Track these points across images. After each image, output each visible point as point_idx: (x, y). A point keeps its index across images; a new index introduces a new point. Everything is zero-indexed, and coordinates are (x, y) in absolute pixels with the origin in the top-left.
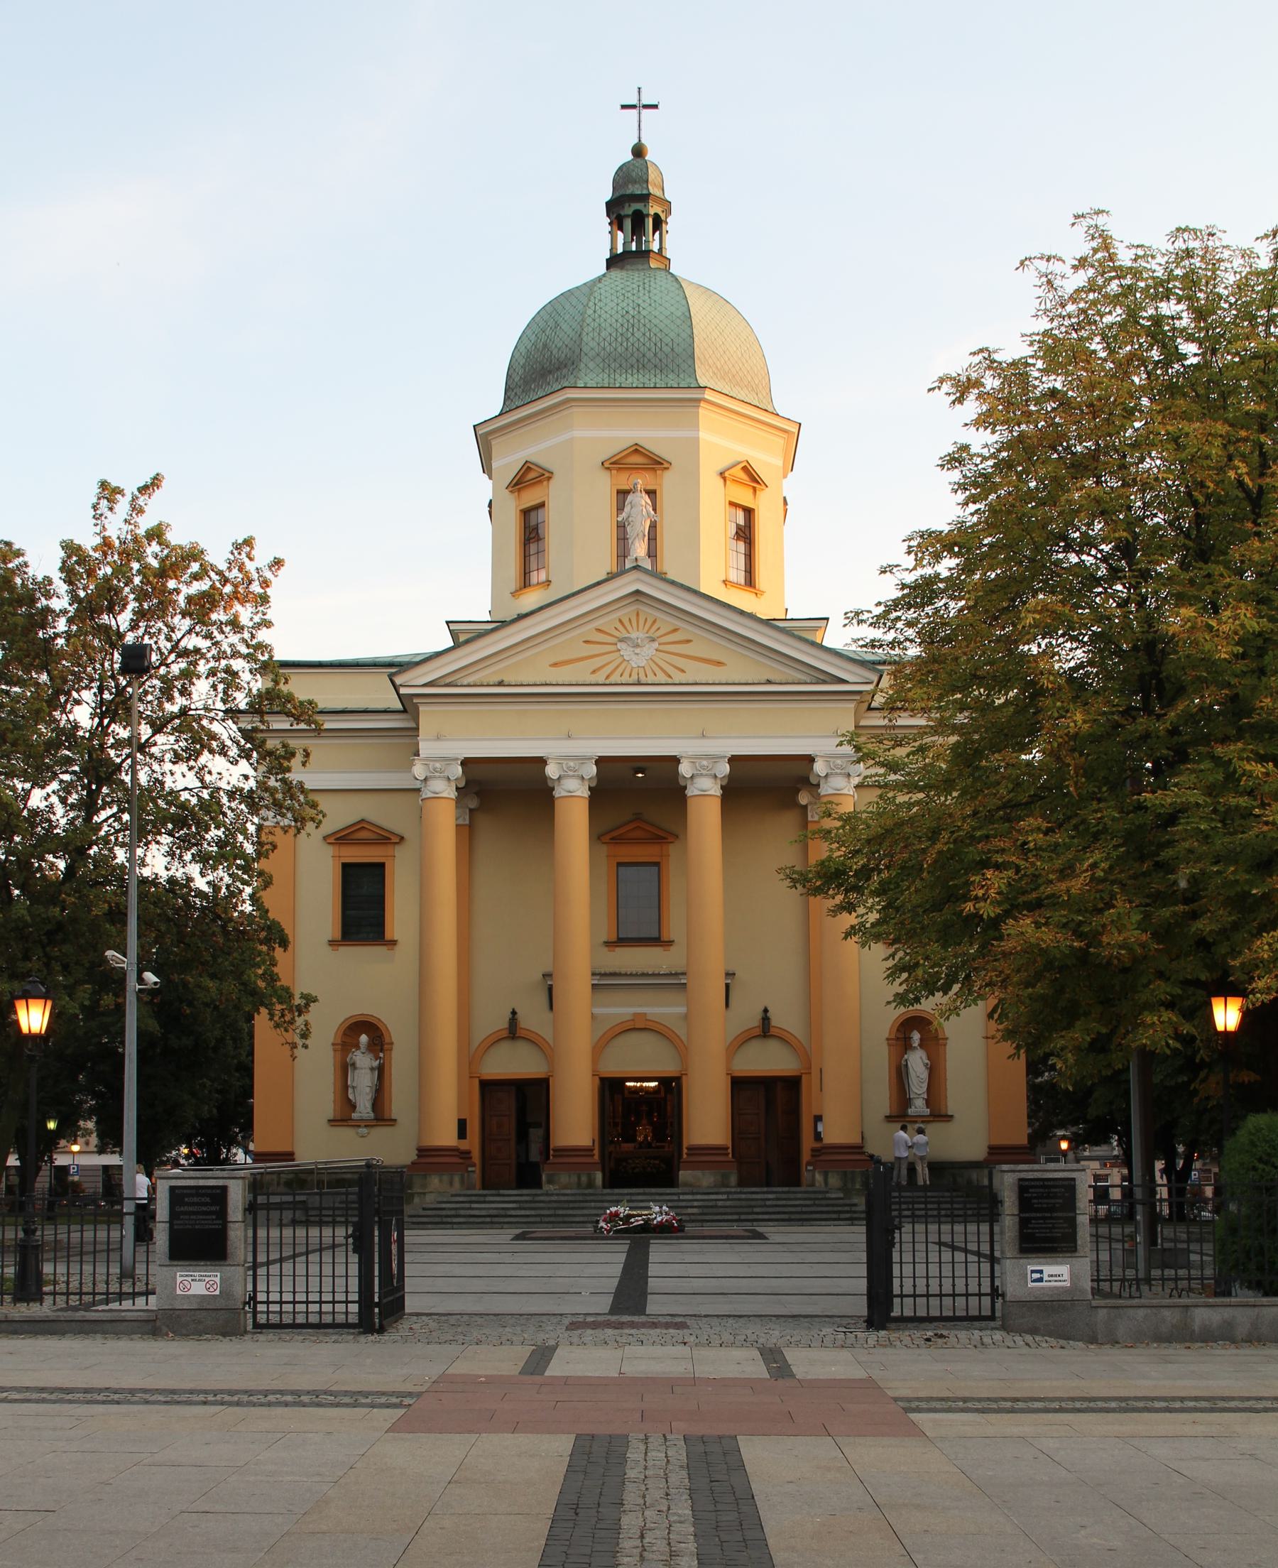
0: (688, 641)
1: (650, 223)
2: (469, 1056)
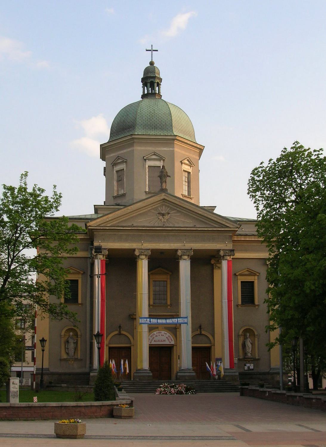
1: (156, 84)
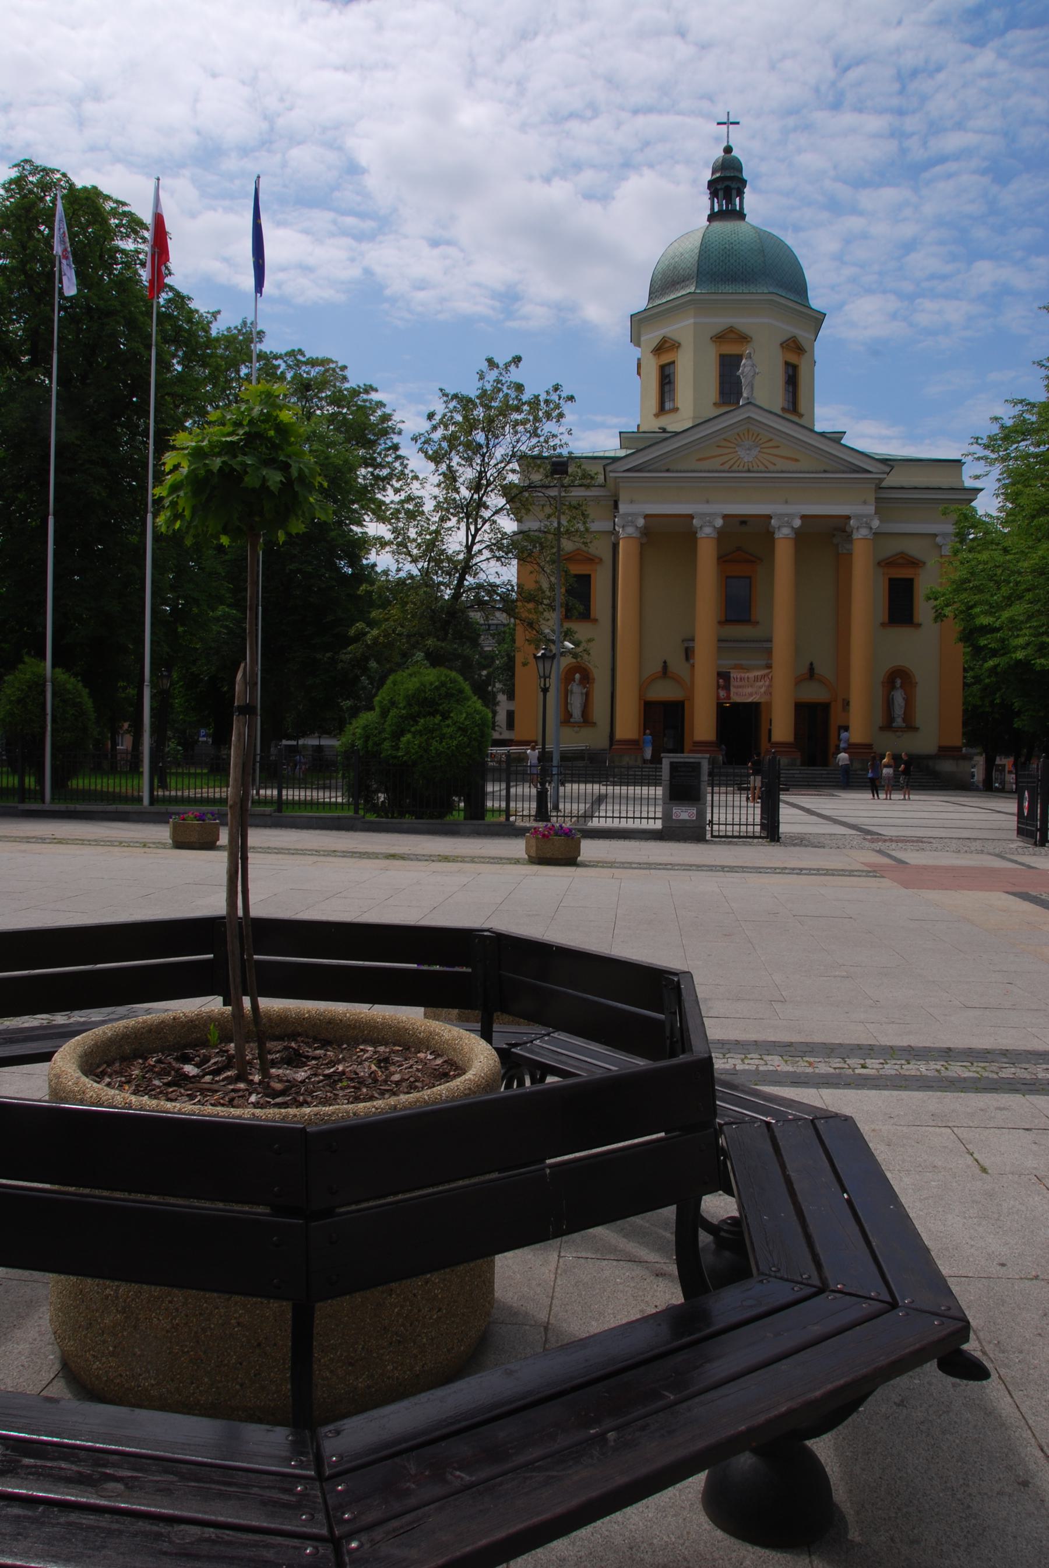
0: (778, 447)
2: (643, 687)
